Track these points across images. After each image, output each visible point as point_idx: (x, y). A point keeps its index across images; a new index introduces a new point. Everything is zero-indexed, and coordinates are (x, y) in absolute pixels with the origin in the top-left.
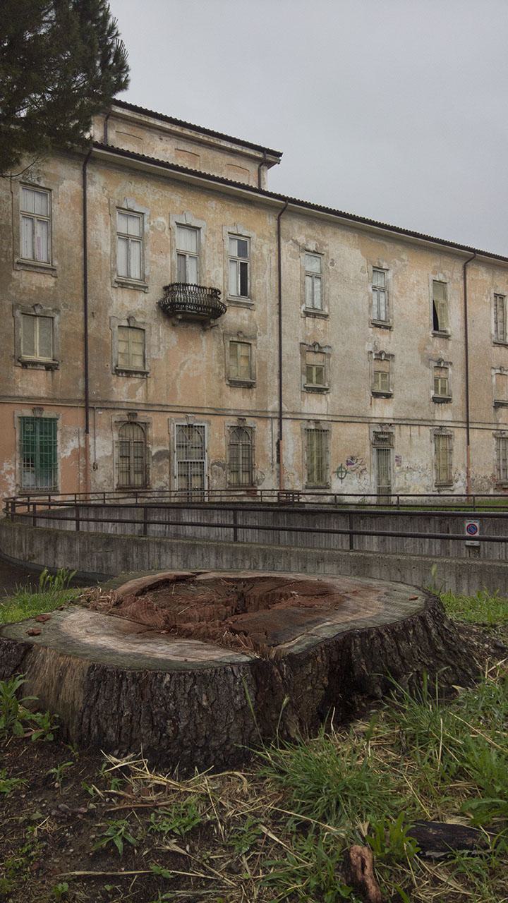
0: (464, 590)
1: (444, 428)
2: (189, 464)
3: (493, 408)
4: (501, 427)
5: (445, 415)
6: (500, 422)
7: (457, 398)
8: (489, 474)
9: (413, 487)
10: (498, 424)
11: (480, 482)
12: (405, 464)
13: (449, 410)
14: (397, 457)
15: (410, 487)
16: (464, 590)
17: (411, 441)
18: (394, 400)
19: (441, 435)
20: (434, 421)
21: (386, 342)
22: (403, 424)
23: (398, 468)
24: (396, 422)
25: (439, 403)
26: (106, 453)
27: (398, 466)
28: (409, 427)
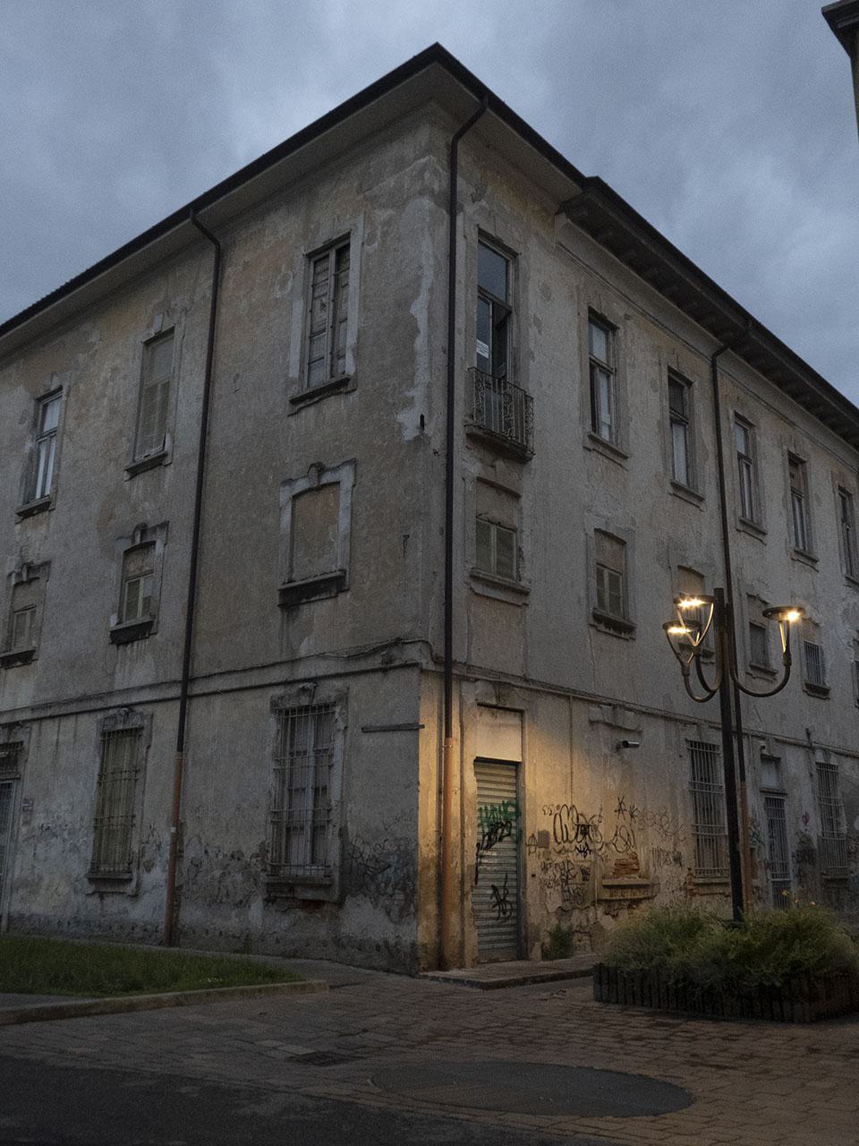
0: (611, 338)
1: (139, 709)
2: (123, 781)
3: (278, 610)
4: (303, 671)
5: (140, 670)
6: (303, 652)
7: (171, 620)
8: (250, 846)
9: (46, 881)
10: (294, 662)
11: (217, 873)
12: (40, 820)
13: (149, 657)
14: (26, 801)
15: (41, 879)
16: (611, 338)
17: (56, 755)
18: (39, 664)
19: (121, 734)
20: (110, 694)
21: (39, 540)
22: (45, 718)
23: (24, 830)
24: (36, 715)
25: (126, 643)
26: (606, 718)
27: (26, 823)
28: (57, 720)
